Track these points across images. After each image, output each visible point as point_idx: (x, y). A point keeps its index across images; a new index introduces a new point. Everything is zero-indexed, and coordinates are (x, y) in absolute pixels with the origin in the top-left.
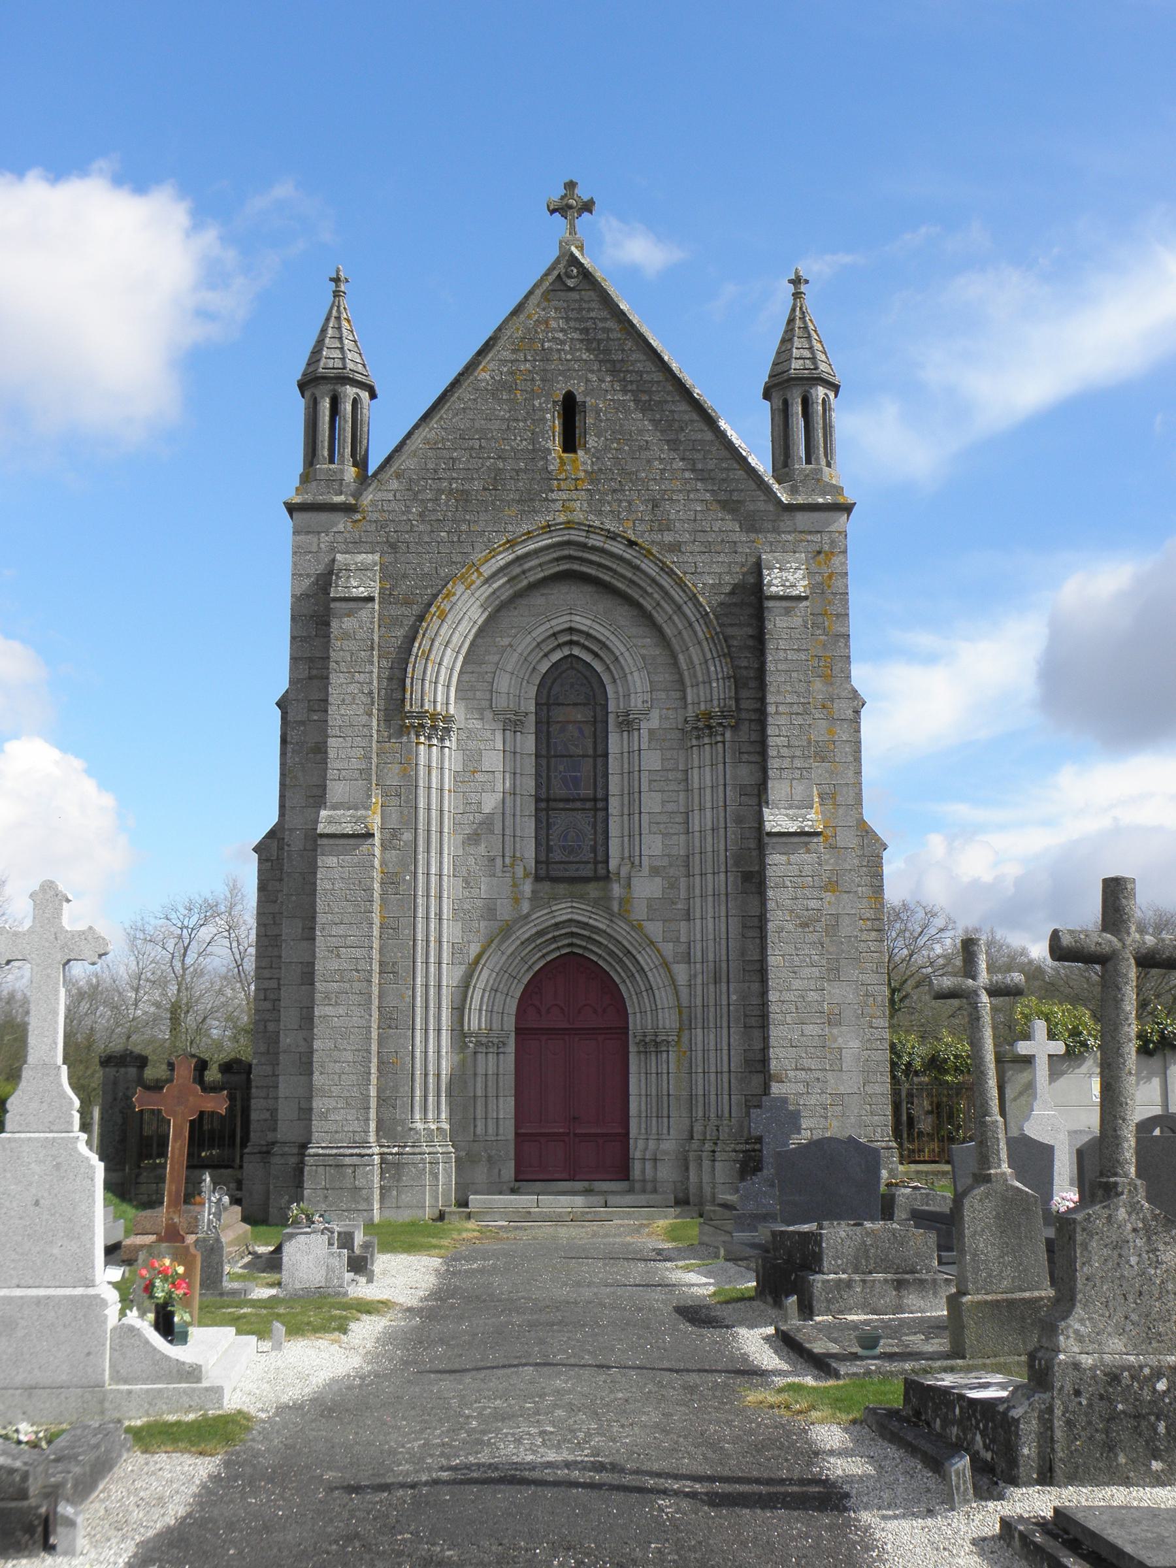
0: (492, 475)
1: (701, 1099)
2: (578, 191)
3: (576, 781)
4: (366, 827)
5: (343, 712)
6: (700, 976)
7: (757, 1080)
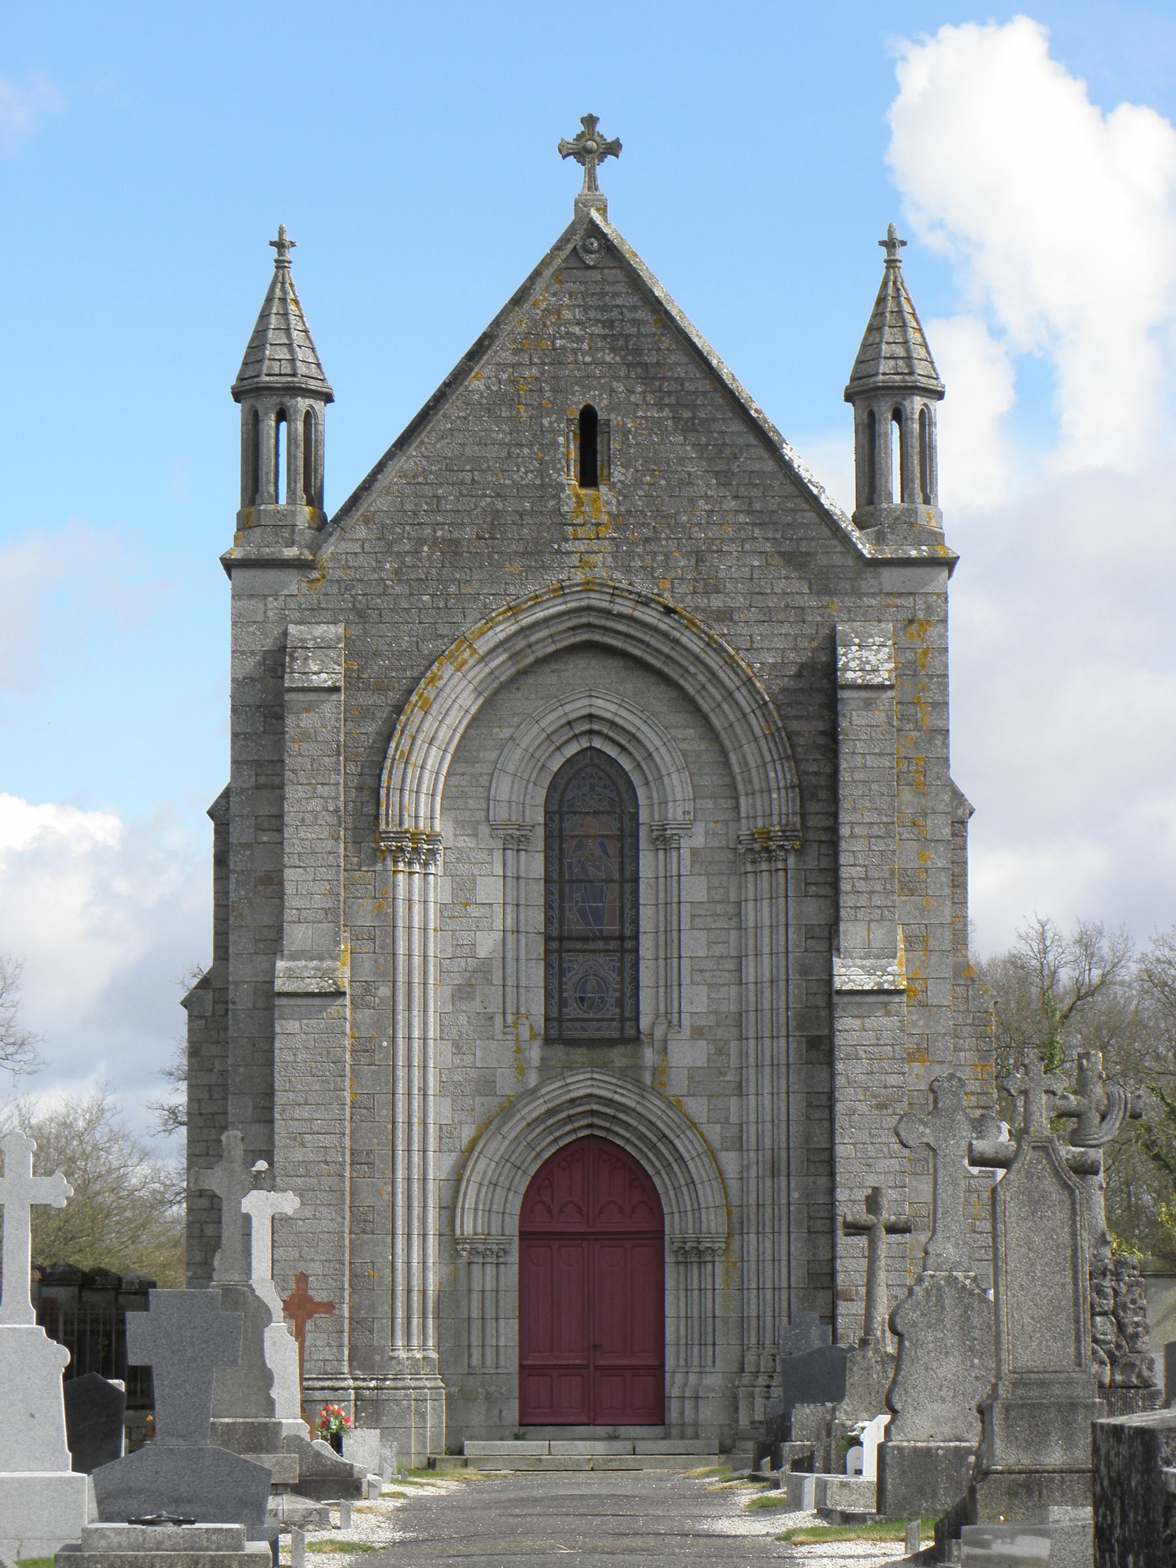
0: (489, 520)
1: (754, 1322)
2: (599, 128)
3: (598, 914)
4: (335, 983)
5: (302, 835)
6: (754, 1168)
7: (823, 1297)
